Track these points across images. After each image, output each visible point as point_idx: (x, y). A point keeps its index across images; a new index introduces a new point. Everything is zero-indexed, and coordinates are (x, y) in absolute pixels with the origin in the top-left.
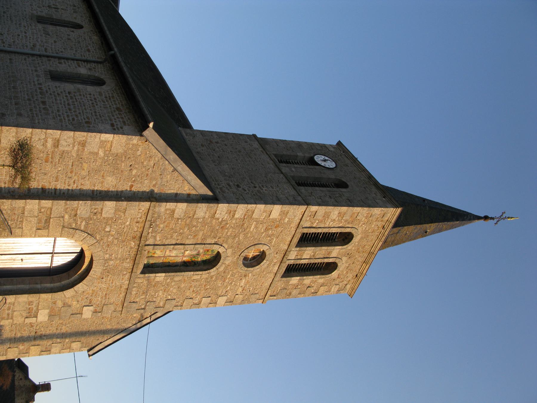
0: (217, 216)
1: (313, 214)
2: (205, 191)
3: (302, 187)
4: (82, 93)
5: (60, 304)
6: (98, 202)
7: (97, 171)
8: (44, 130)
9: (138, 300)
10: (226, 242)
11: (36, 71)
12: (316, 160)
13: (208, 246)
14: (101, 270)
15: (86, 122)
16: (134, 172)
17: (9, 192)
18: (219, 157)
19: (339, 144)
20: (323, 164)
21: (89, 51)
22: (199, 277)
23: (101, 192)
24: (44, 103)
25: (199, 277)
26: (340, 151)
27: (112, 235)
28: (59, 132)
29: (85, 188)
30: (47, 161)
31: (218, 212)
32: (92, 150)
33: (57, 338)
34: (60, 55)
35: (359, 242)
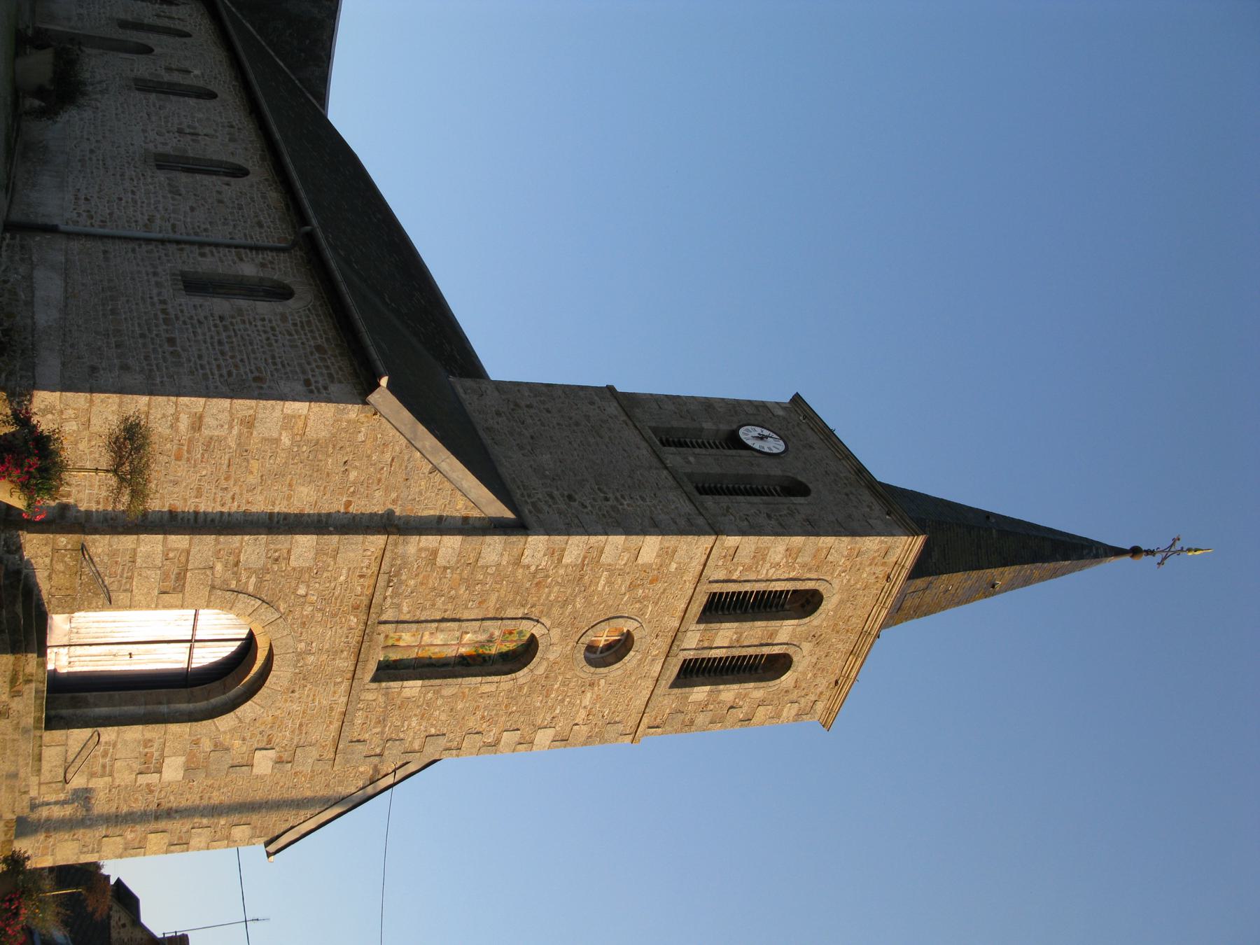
0: (526, 560)
1: (731, 552)
2: (498, 509)
3: (709, 497)
4: (246, 318)
5: (207, 745)
6: (281, 537)
7: (278, 475)
8: (173, 399)
9: (367, 736)
10: (548, 615)
11: (155, 274)
12: (742, 436)
13: (509, 622)
14: (289, 675)
15: (256, 379)
16: (353, 475)
17: (106, 520)
18: (532, 437)
19: (797, 399)
20: (757, 445)
21: (260, 225)
22: (493, 688)
23: (286, 516)
24: (171, 341)
25: (493, 688)
26: (797, 417)
27: (312, 603)
28: (202, 401)
29: (254, 509)
30: (178, 458)
31: (526, 552)
32: (266, 435)
33: (203, 816)
34: (202, 238)
35: (835, 611)
